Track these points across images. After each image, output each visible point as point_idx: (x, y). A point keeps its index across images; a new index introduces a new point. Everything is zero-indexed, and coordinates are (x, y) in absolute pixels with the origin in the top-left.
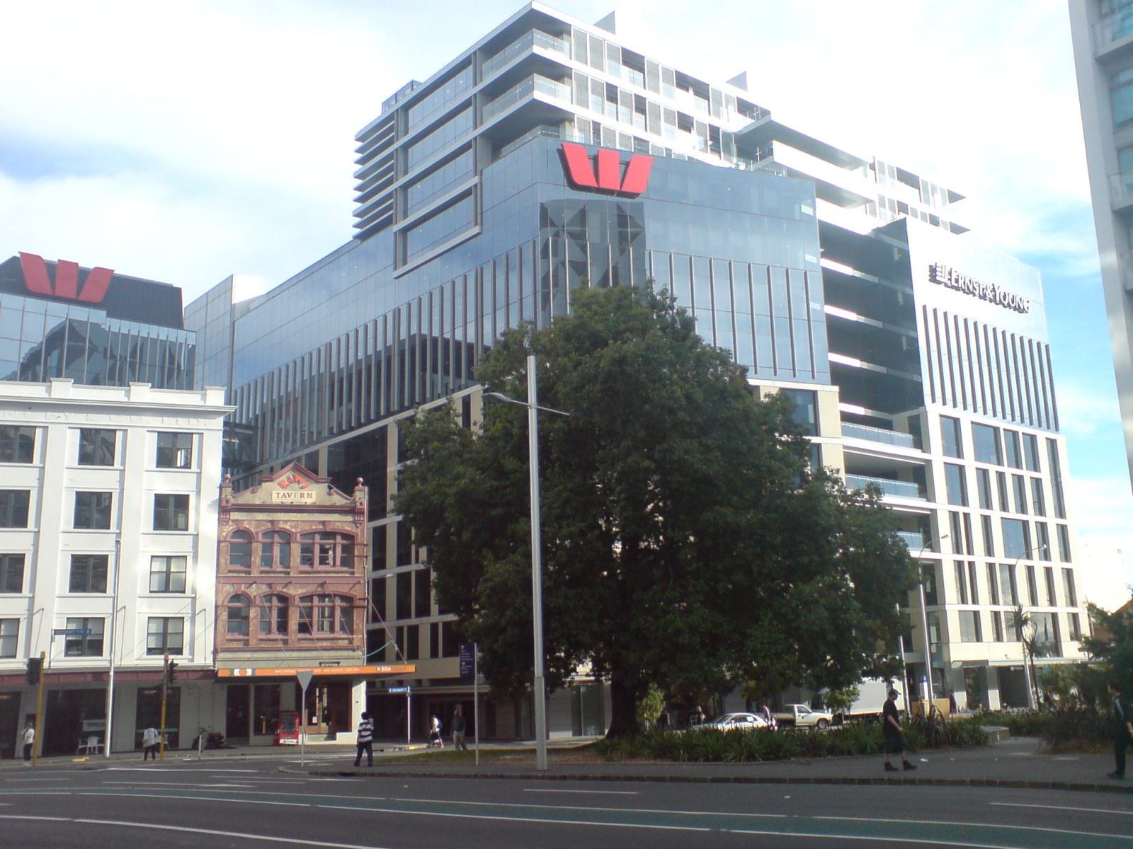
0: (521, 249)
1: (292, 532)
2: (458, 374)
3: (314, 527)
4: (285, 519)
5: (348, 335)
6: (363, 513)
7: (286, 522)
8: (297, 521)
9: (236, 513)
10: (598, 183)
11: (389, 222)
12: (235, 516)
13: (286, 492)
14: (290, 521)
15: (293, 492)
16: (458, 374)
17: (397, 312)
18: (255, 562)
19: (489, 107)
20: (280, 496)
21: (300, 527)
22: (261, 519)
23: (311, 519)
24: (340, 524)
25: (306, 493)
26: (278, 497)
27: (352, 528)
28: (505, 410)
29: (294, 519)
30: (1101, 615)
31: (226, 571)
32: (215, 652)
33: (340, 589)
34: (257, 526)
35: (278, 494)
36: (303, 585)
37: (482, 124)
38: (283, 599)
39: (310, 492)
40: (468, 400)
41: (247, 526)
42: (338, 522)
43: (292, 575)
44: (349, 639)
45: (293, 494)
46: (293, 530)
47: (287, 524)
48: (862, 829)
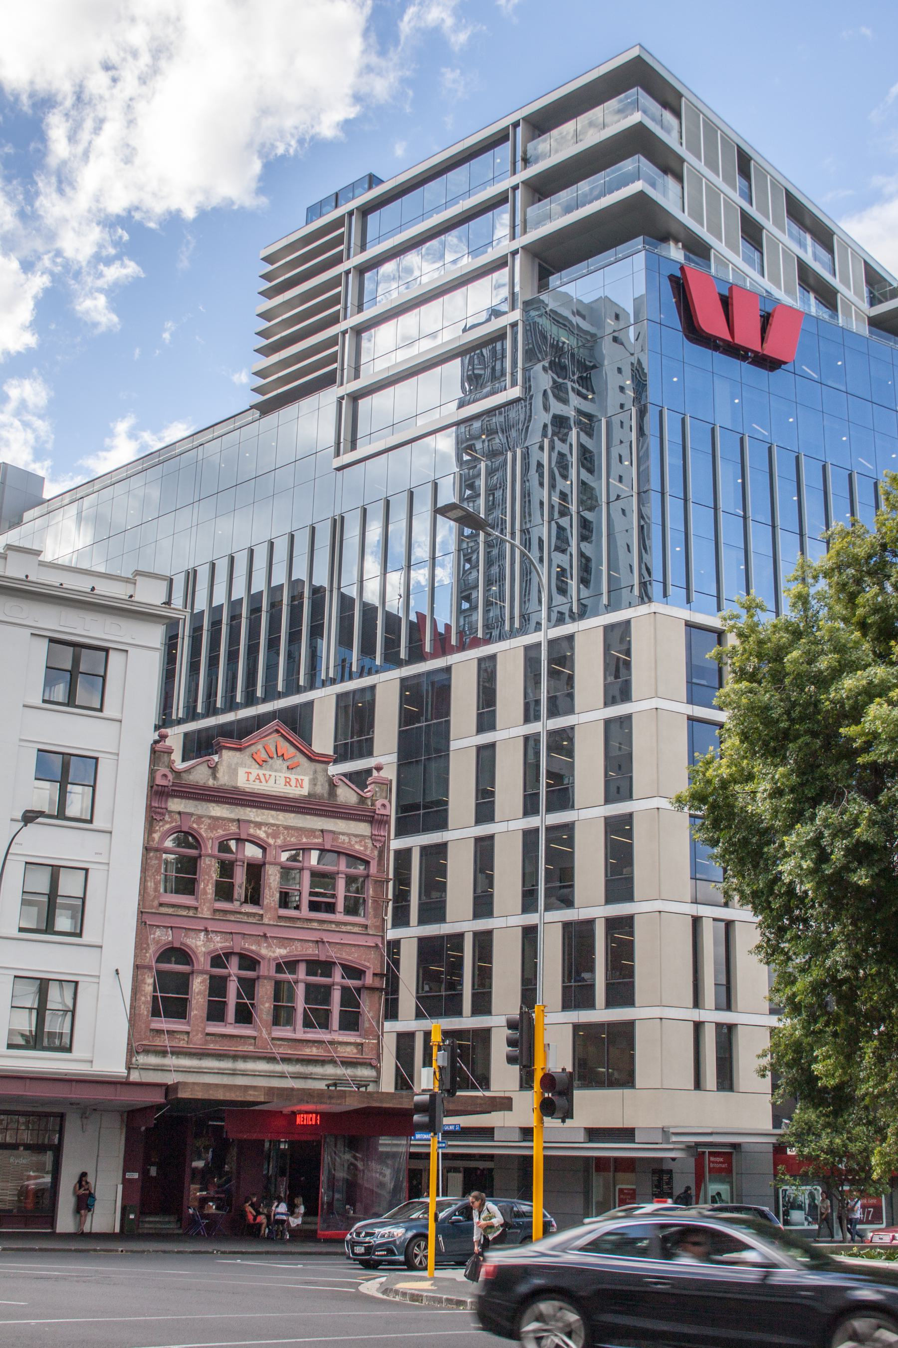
0: (388, 503)
1: (270, 845)
2: (368, 649)
3: (304, 840)
4: (258, 819)
5: (213, 566)
6: (388, 822)
7: (259, 825)
8: (278, 826)
9: (176, 800)
10: (732, 336)
11: (329, 380)
12: (176, 805)
13: (261, 772)
14: (266, 824)
15: (273, 774)
16: (368, 649)
17: (191, 576)
18: (205, 893)
19: (533, 211)
20: (252, 778)
21: (282, 838)
22: (218, 815)
23: (300, 825)
24: (346, 839)
25: (293, 777)
26: (248, 780)
27: (366, 847)
28: (785, 637)
29: (272, 821)
30: (568, 1088)
31: (156, 903)
32: (132, 1051)
33: (344, 956)
34: (212, 828)
35: (249, 773)
36: (284, 941)
37: (525, 232)
38: (249, 962)
39: (299, 777)
40: (368, 697)
41: (195, 826)
42: (343, 834)
43: (266, 921)
44: (357, 1045)
45: (273, 779)
46: (271, 841)
47: (260, 829)
48: (22, 1269)
